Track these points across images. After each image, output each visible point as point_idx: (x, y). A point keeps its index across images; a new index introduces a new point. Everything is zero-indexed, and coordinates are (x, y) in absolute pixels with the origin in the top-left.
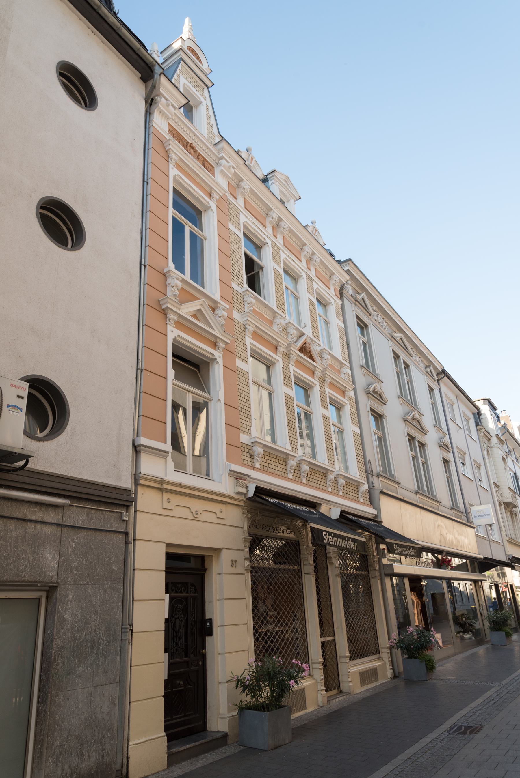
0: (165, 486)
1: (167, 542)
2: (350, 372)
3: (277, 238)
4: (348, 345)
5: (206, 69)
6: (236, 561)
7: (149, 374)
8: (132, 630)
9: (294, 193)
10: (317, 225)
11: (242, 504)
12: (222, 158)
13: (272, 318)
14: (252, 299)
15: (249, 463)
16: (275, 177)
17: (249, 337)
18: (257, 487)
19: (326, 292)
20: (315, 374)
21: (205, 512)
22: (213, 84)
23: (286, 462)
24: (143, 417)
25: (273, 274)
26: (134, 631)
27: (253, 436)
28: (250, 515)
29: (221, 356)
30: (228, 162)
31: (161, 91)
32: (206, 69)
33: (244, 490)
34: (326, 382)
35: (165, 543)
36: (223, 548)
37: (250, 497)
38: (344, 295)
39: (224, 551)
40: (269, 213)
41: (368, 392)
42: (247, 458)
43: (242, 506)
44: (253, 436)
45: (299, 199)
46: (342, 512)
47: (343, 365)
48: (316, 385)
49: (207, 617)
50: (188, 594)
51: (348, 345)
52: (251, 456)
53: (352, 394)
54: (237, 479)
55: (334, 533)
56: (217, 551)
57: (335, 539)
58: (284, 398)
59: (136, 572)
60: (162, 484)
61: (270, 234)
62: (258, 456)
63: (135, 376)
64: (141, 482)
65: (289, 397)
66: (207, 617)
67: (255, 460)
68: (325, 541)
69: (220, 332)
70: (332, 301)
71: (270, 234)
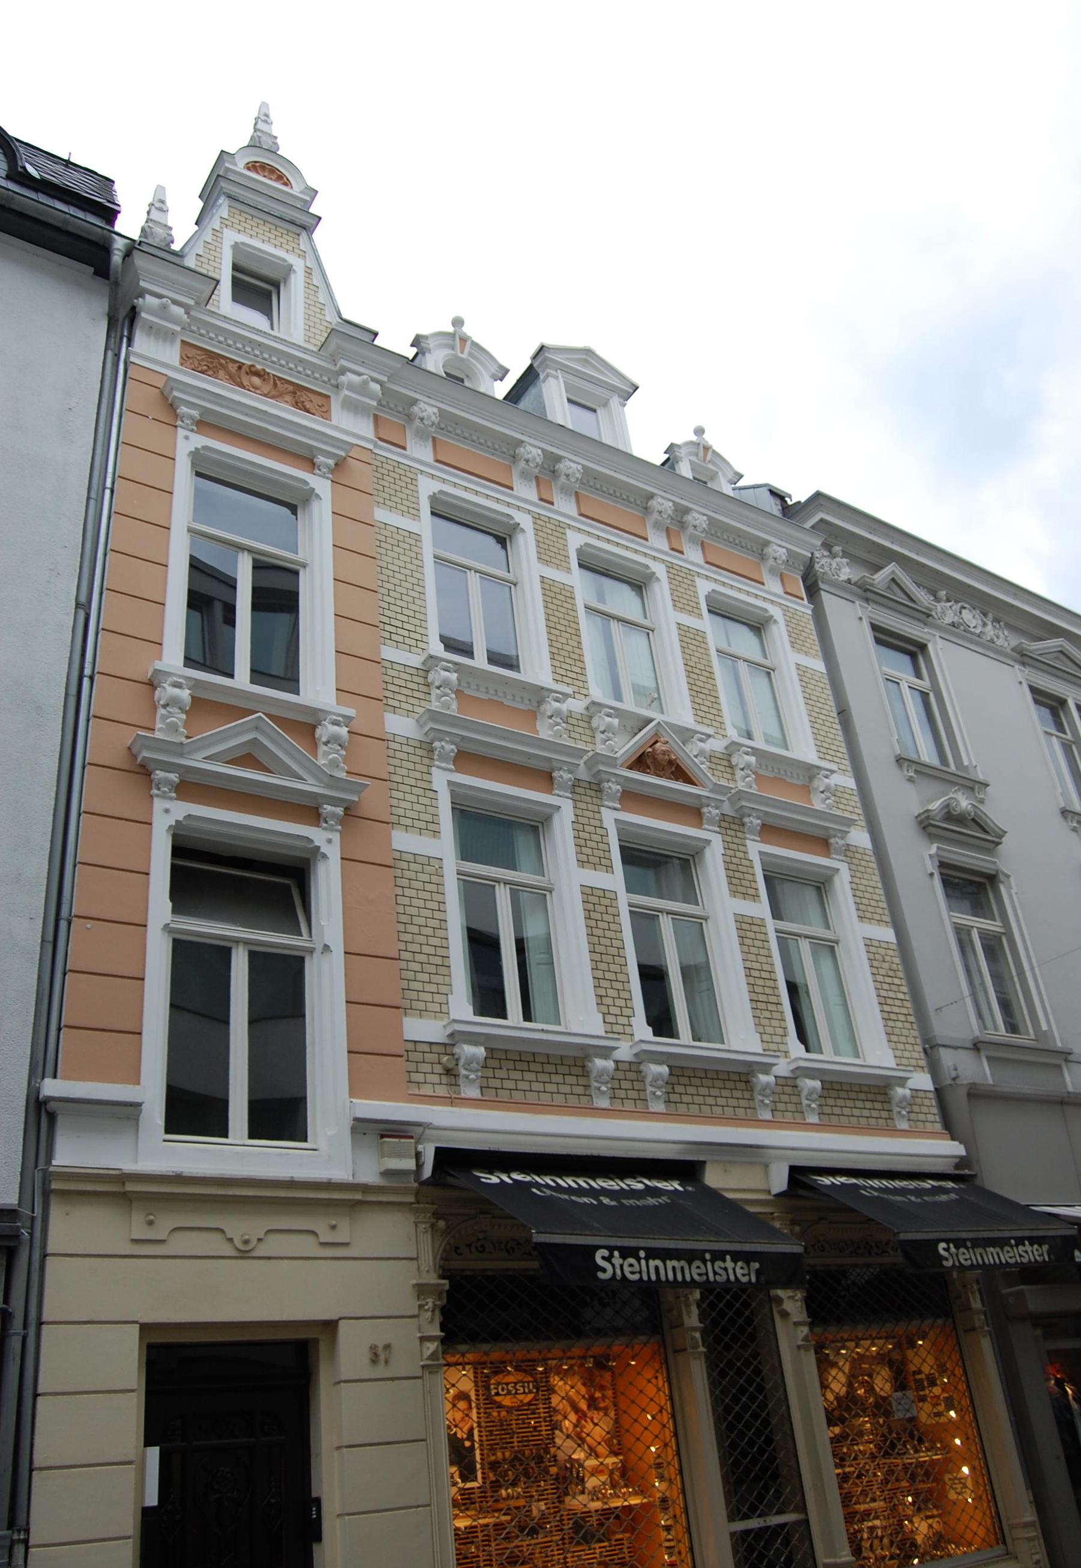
0: (130, 1187)
1: (142, 1321)
2: (850, 783)
3: (682, 553)
4: (844, 715)
5: (301, 192)
6: (387, 1347)
7: (89, 924)
8: (26, 1542)
9: (616, 383)
10: (709, 438)
11: (412, 1199)
12: (343, 371)
13: (807, 780)
14: (747, 757)
15: (442, 1091)
16: (548, 362)
17: (754, 840)
18: (437, 1149)
19: (748, 593)
20: (704, 814)
21: (178, 1235)
22: (320, 218)
23: (583, 1067)
24: (67, 1029)
25: (796, 678)
26: (32, 1542)
27: (637, 1038)
28: (442, 1224)
29: (336, 837)
30: (360, 374)
31: (142, 284)
32: (301, 192)
33: (410, 1164)
34: (747, 827)
35: (136, 1322)
36: (340, 1319)
37: (428, 1179)
38: (822, 586)
39: (342, 1323)
40: (517, 451)
41: (926, 823)
42: (435, 1079)
43: (412, 1203)
44: (637, 1038)
45: (634, 391)
46: (793, 1170)
47: (816, 771)
48: (708, 842)
49: (314, 1495)
50: (252, 1440)
51: (844, 715)
52: (450, 1072)
53: (860, 838)
54: (382, 1136)
55: (970, 1240)
56: (330, 1327)
57: (978, 1251)
58: (733, 926)
59: (40, 1399)
60: (124, 1183)
61: (779, 596)
62: (599, 1079)
63: (952, 1050)
64: (54, 1186)
65: (875, 943)
66: (314, 1495)
67: (461, 1081)
68: (948, 1264)
69: (320, 781)
70: (776, 612)
71: (779, 596)
